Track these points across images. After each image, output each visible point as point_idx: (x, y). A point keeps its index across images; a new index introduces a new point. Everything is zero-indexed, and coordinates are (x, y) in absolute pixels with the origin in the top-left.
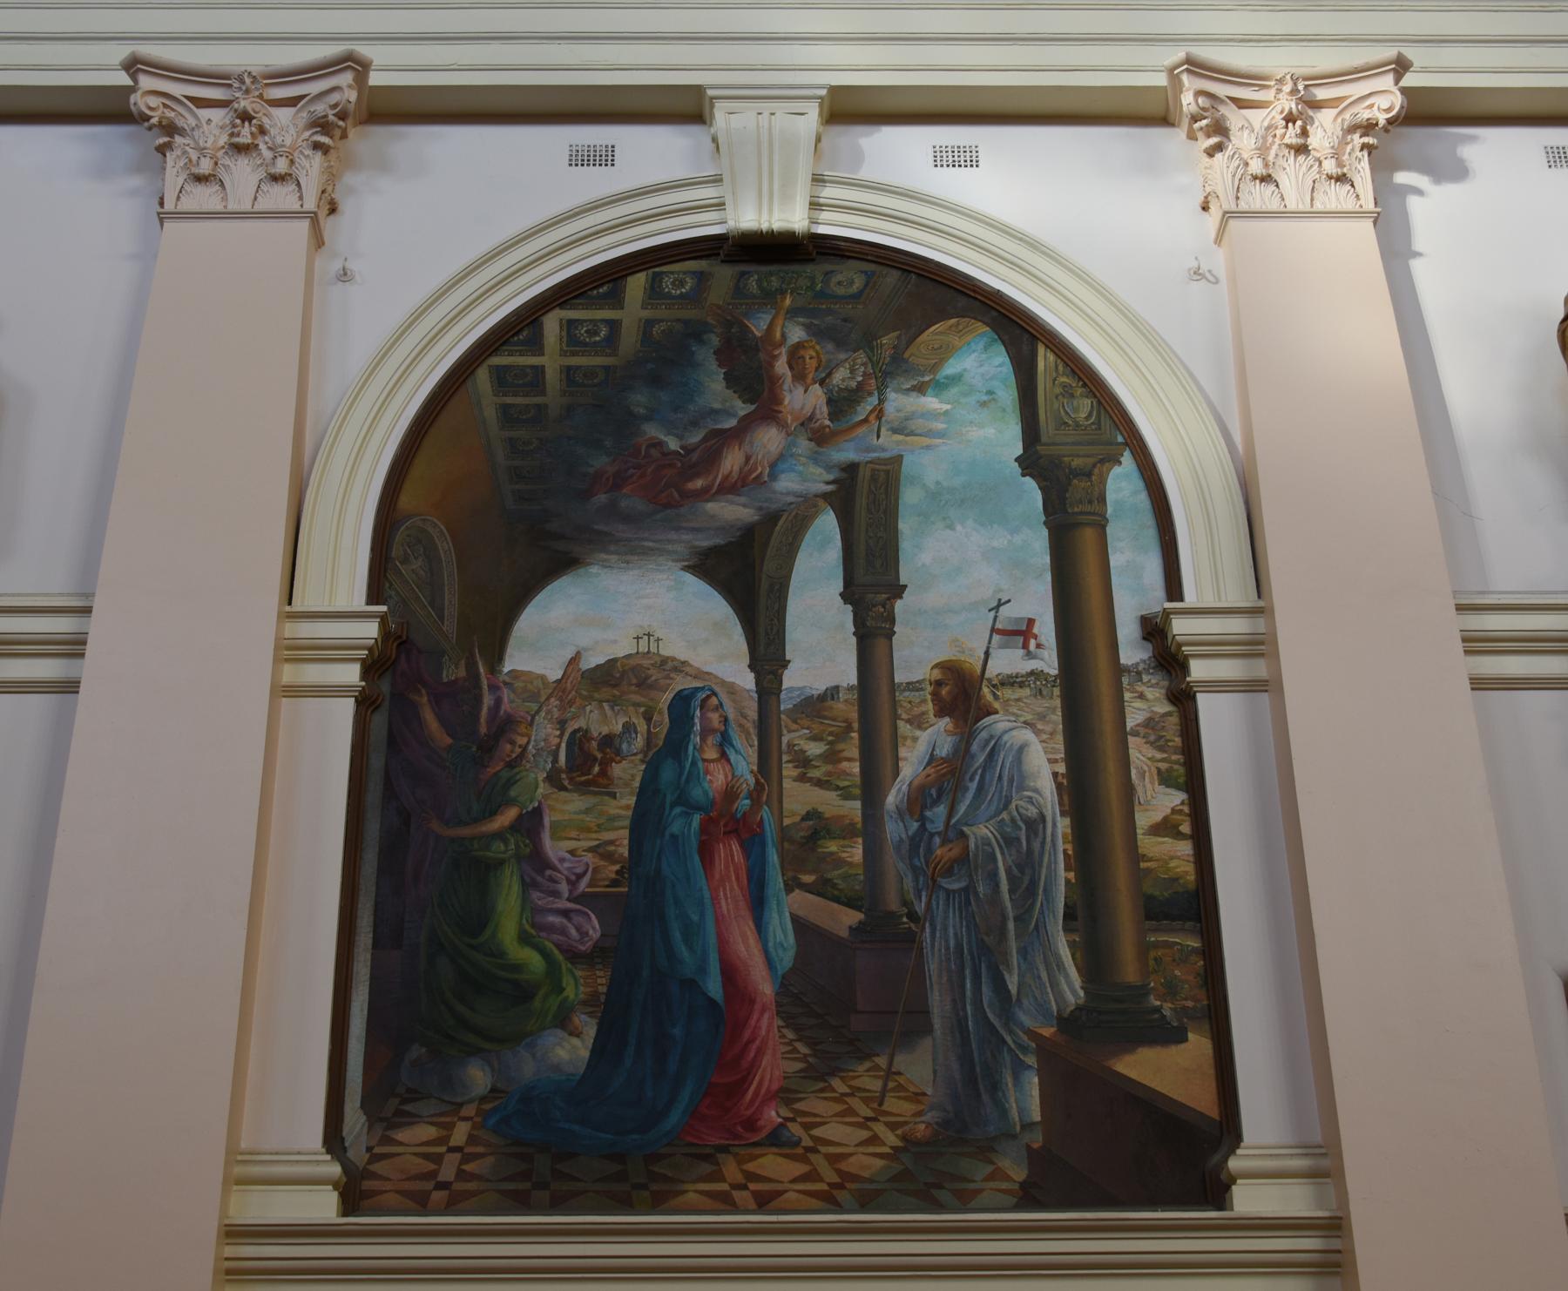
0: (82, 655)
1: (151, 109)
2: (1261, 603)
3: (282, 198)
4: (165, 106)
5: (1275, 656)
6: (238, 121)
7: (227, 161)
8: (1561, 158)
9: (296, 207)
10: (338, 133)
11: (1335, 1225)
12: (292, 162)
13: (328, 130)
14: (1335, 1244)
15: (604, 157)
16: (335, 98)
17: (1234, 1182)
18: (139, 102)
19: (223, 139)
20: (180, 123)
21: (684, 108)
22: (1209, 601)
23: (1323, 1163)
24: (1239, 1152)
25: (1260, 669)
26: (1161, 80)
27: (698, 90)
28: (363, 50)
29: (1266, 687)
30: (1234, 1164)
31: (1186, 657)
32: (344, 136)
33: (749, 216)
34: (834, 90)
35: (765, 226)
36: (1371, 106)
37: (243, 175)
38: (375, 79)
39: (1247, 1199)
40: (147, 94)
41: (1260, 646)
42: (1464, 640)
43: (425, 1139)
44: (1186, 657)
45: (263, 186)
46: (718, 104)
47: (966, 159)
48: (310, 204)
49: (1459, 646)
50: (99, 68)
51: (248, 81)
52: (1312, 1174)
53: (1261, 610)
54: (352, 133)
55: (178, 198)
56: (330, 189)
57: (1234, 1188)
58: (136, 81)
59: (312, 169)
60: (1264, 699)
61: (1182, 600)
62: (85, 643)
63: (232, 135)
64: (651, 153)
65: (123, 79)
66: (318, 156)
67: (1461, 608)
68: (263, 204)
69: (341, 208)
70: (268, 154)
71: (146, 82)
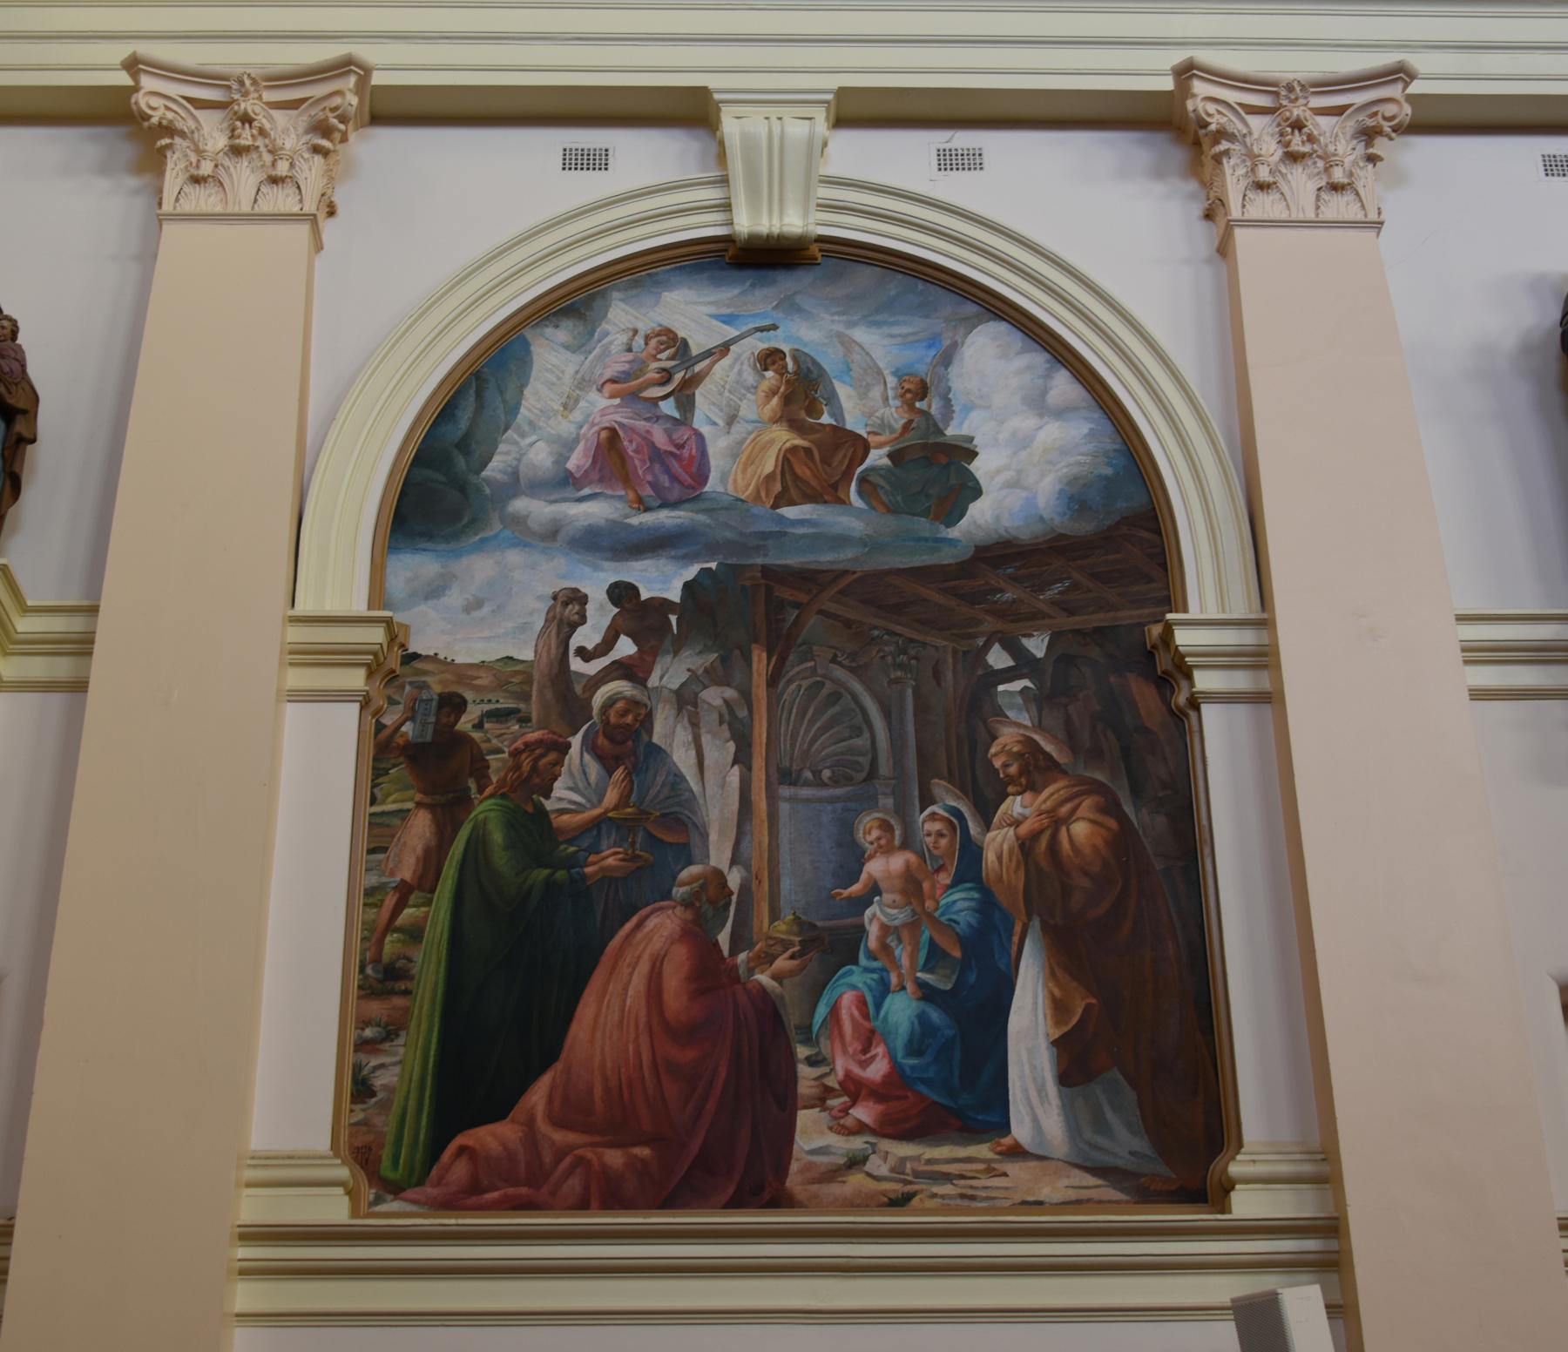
0: (90, 654)
1: (1209, 115)
2: (1265, 616)
3: (282, 200)
4: (167, 108)
5: (1277, 667)
6: (238, 124)
7: (227, 162)
8: (1555, 167)
9: (296, 209)
10: (337, 136)
11: (1333, 1227)
12: (292, 165)
13: (325, 133)
14: (1333, 1245)
15: (595, 161)
16: (337, 101)
17: (1233, 1188)
18: (142, 101)
19: (1279, 153)
20: (180, 125)
21: (689, 111)
22: (1213, 613)
23: (1323, 1169)
24: (1239, 1157)
25: (1264, 682)
26: (1167, 84)
27: (703, 93)
28: (366, 53)
29: (1269, 699)
30: (1234, 1169)
31: (1190, 668)
32: (344, 139)
33: (747, 222)
34: (842, 93)
35: (776, 230)
36: (1375, 114)
37: (244, 178)
38: (378, 79)
39: (1246, 1204)
40: (153, 97)
41: (1264, 658)
42: (1463, 650)
43: (1033, 1164)
44: (1190, 668)
45: (263, 189)
46: (725, 109)
47: (970, 161)
48: (310, 207)
49: (1459, 656)
50: (99, 67)
51: (248, 82)
52: (1318, 1180)
53: (1265, 623)
54: (352, 137)
55: (177, 200)
56: (329, 192)
57: (1233, 1195)
58: (137, 81)
59: (312, 172)
60: (1267, 710)
61: (1186, 611)
62: (92, 642)
63: (232, 137)
64: (644, 158)
65: (124, 79)
66: (318, 159)
67: (1462, 619)
68: (265, 207)
69: (340, 210)
70: (268, 158)
71: (148, 83)
